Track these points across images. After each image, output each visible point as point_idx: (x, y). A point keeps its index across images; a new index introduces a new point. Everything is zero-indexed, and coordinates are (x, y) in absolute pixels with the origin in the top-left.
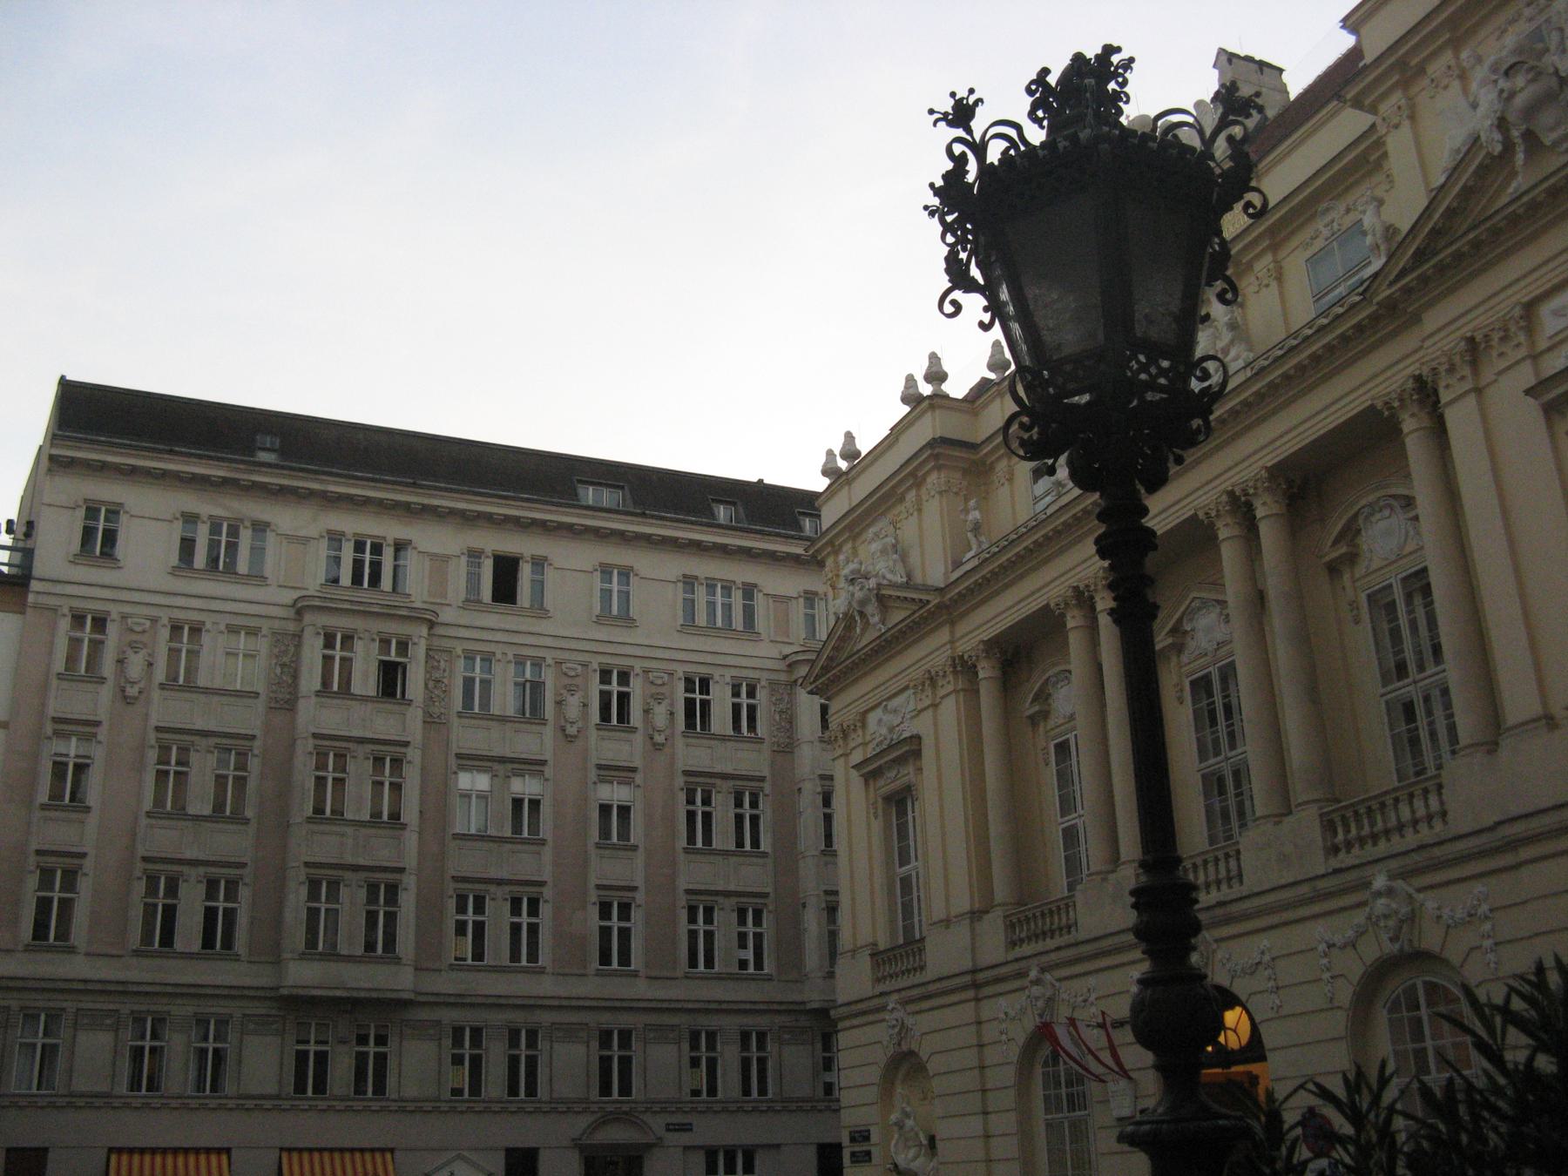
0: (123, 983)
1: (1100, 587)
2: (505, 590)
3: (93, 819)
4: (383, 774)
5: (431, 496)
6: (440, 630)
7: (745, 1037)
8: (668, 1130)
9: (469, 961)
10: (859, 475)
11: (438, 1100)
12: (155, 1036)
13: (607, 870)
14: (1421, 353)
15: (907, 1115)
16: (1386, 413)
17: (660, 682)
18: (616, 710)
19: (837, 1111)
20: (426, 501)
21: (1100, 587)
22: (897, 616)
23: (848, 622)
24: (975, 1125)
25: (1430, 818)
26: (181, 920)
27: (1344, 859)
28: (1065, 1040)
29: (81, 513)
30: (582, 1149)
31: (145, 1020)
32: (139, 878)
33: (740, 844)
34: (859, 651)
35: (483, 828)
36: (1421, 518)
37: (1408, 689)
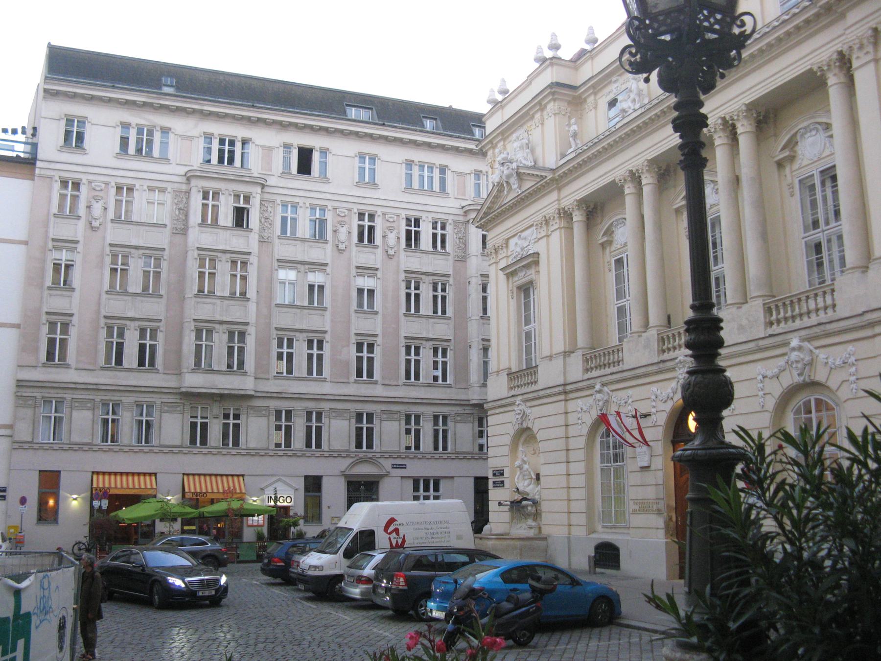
0: (96, 384)
1: (644, 171)
2: (305, 166)
3: (76, 294)
4: (236, 270)
5: (262, 113)
6: (267, 190)
7: (436, 418)
8: (393, 468)
9: (285, 374)
10: (507, 103)
11: (268, 449)
12: (114, 413)
13: (362, 324)
14: (843, 38)
15: (525, 462)
16: (819, 74)
17: (392, 220)
18: (367, 236)
19: (487, 459)
20: (260, 116)
21: (644, 171)
22: (528, 184)
23: (500, 187)
24: (562, 468)
25: (826, 308)
26: (126, 351)
27: (775, 329)
28: (614, 424)
29: (64, 122)
30: (346, 476)
31: (108, 405)
32: (103, 328)
33: (435, 312)
34: (505, 204)
35: (292, 301)
36: (834, 136)
37: (819, 235)
